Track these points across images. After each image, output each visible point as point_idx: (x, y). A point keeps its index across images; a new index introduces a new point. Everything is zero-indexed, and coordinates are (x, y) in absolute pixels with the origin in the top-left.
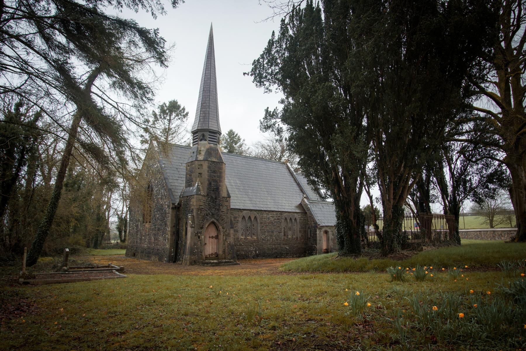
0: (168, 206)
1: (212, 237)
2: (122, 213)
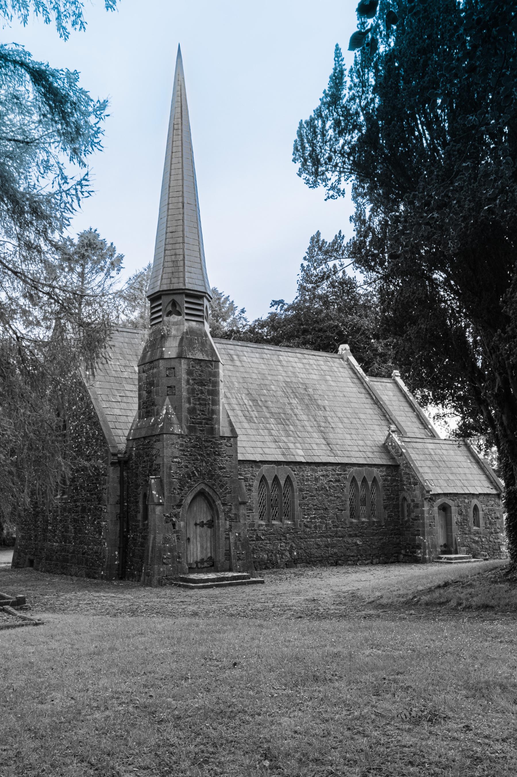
1: (202, 525)
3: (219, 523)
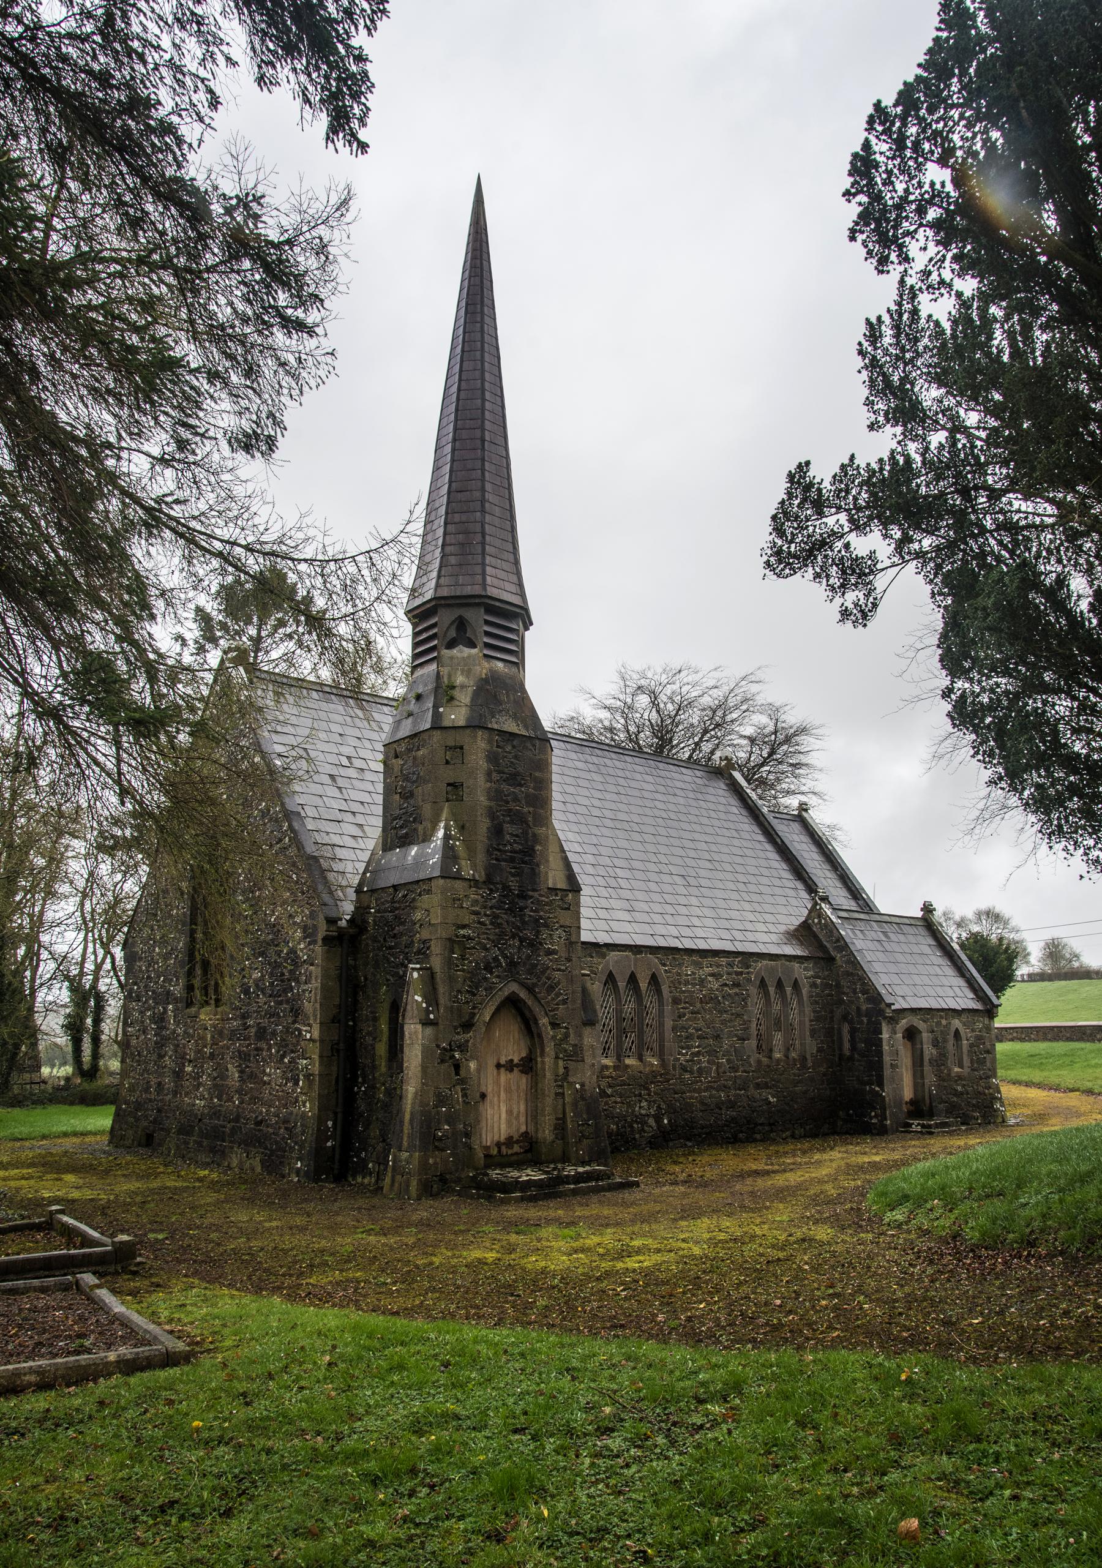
0: (309, 933)
1: (510, 1066)
2: (82, 973)
3: (543, 1063)
